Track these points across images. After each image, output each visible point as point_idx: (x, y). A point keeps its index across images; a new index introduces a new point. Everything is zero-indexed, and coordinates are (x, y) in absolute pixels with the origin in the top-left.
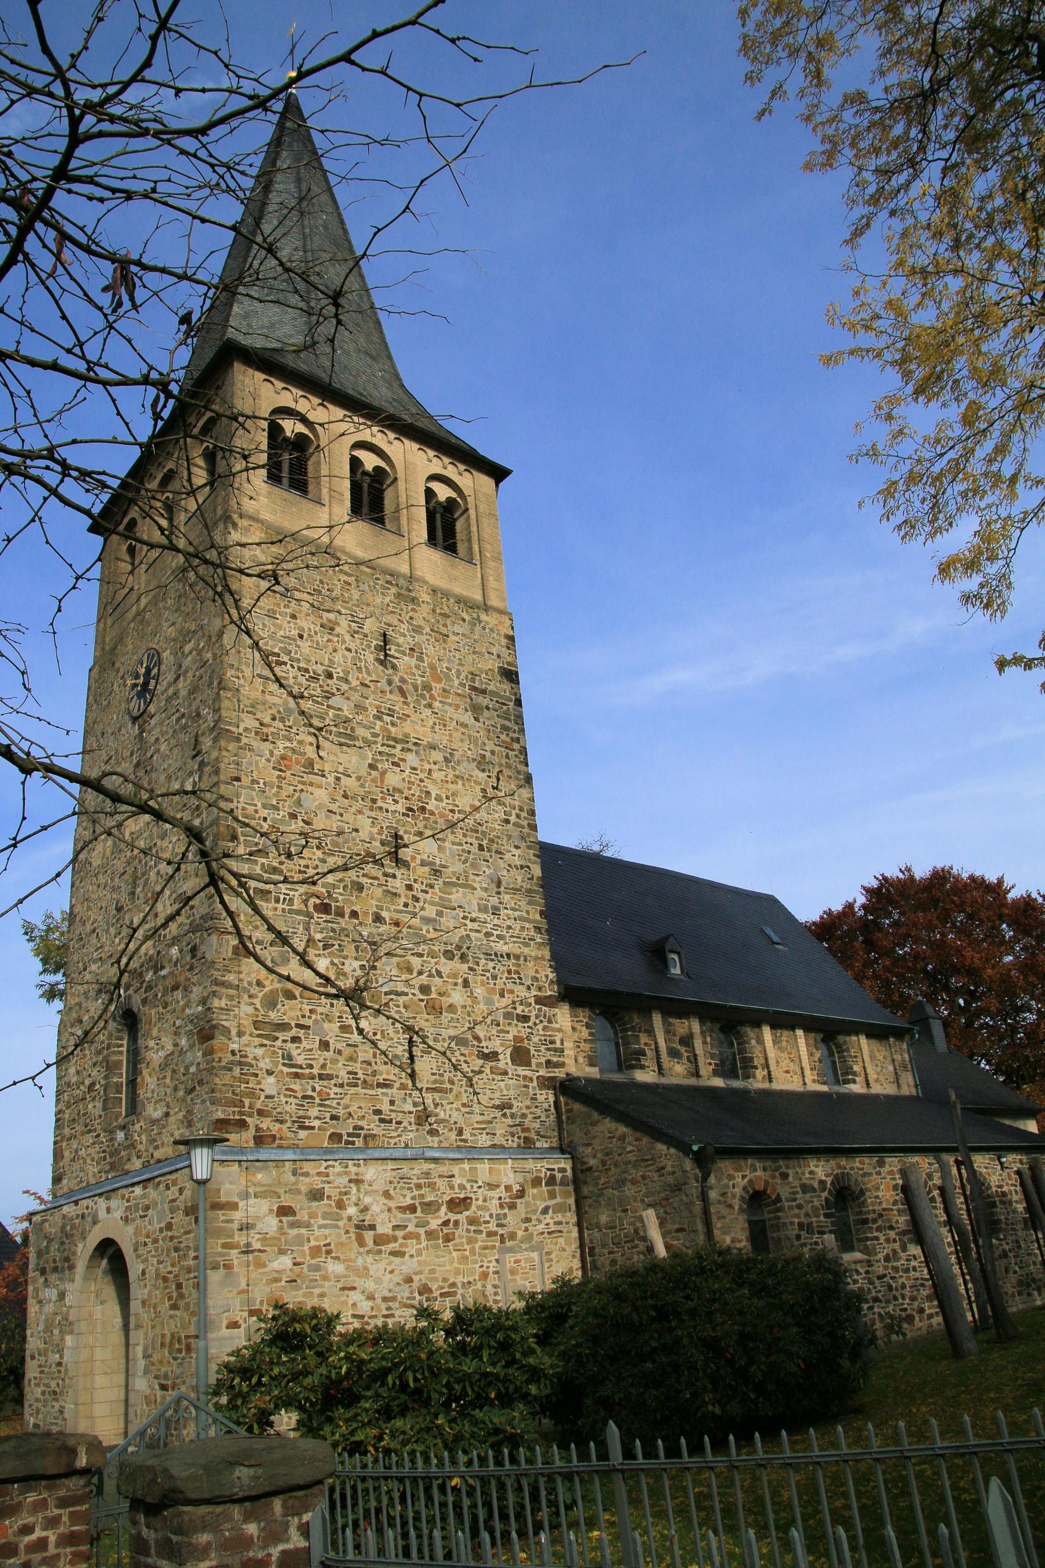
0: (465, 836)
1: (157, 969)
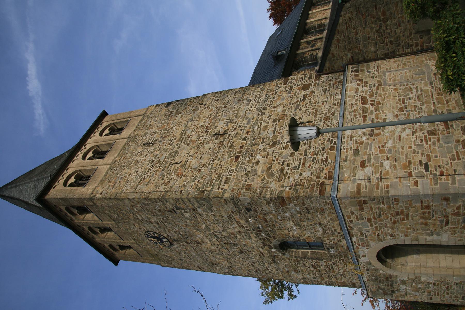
0: (220, 113)
1: (260, 231)
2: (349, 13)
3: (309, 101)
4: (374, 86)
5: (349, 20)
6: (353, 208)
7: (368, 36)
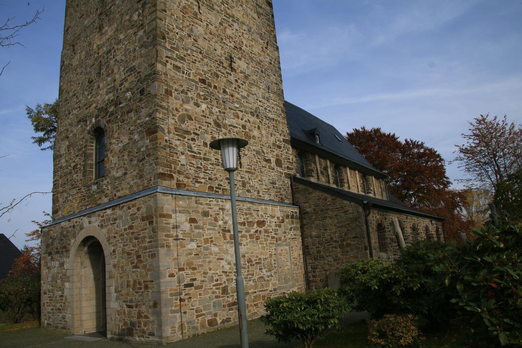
0: (256, 65)
1: (116, 105)
2: (352, 210)
3: (264, 166)
4: (276, 234)
5: (346, 210)
6: (145, 209)
7: (327, 230)
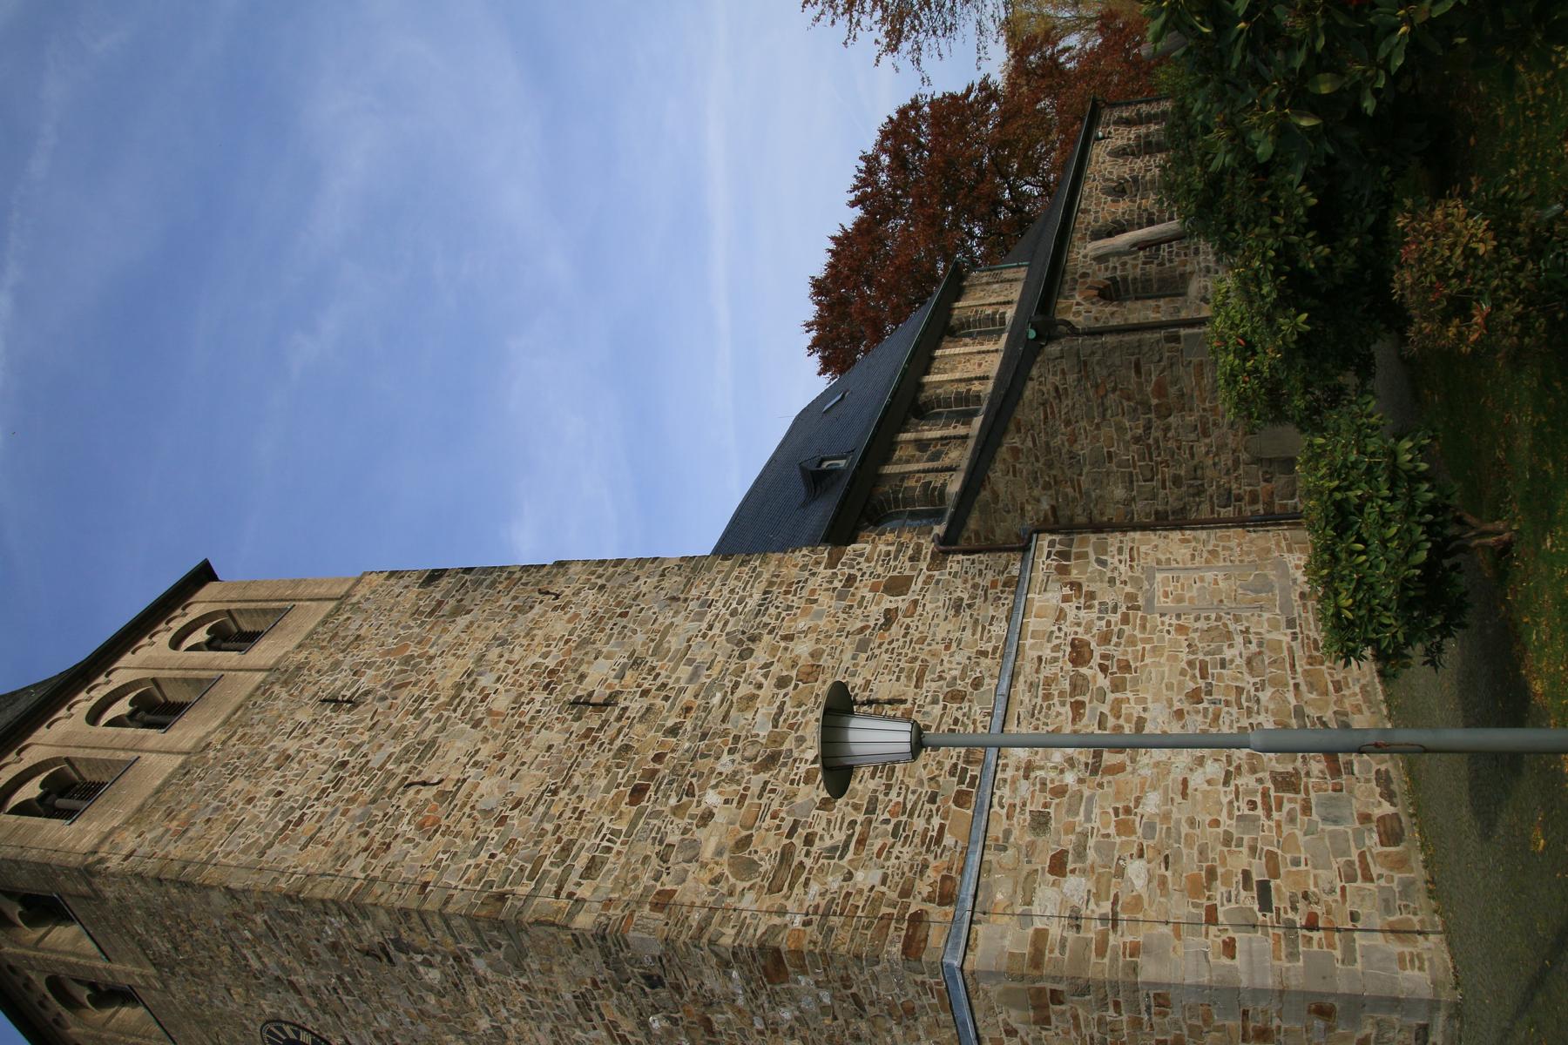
0: (602, 630)
